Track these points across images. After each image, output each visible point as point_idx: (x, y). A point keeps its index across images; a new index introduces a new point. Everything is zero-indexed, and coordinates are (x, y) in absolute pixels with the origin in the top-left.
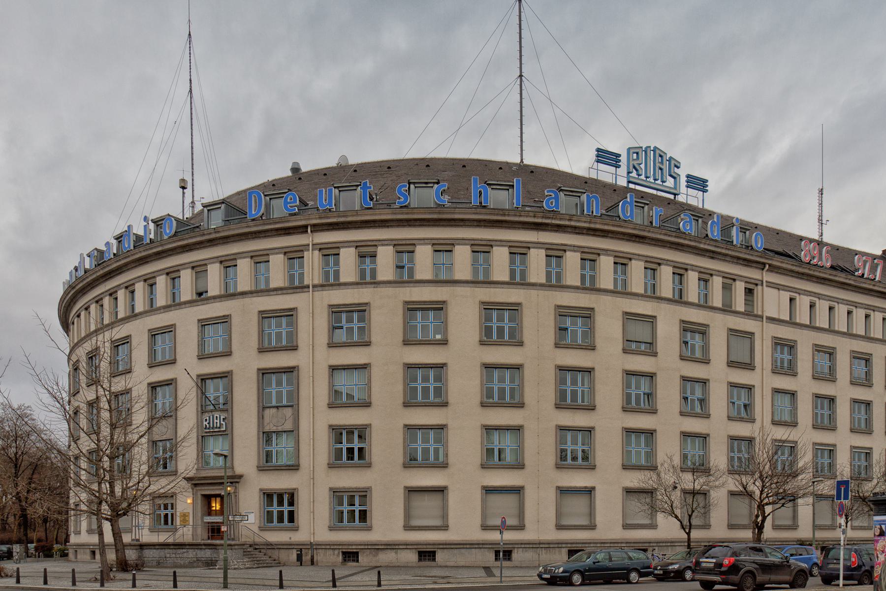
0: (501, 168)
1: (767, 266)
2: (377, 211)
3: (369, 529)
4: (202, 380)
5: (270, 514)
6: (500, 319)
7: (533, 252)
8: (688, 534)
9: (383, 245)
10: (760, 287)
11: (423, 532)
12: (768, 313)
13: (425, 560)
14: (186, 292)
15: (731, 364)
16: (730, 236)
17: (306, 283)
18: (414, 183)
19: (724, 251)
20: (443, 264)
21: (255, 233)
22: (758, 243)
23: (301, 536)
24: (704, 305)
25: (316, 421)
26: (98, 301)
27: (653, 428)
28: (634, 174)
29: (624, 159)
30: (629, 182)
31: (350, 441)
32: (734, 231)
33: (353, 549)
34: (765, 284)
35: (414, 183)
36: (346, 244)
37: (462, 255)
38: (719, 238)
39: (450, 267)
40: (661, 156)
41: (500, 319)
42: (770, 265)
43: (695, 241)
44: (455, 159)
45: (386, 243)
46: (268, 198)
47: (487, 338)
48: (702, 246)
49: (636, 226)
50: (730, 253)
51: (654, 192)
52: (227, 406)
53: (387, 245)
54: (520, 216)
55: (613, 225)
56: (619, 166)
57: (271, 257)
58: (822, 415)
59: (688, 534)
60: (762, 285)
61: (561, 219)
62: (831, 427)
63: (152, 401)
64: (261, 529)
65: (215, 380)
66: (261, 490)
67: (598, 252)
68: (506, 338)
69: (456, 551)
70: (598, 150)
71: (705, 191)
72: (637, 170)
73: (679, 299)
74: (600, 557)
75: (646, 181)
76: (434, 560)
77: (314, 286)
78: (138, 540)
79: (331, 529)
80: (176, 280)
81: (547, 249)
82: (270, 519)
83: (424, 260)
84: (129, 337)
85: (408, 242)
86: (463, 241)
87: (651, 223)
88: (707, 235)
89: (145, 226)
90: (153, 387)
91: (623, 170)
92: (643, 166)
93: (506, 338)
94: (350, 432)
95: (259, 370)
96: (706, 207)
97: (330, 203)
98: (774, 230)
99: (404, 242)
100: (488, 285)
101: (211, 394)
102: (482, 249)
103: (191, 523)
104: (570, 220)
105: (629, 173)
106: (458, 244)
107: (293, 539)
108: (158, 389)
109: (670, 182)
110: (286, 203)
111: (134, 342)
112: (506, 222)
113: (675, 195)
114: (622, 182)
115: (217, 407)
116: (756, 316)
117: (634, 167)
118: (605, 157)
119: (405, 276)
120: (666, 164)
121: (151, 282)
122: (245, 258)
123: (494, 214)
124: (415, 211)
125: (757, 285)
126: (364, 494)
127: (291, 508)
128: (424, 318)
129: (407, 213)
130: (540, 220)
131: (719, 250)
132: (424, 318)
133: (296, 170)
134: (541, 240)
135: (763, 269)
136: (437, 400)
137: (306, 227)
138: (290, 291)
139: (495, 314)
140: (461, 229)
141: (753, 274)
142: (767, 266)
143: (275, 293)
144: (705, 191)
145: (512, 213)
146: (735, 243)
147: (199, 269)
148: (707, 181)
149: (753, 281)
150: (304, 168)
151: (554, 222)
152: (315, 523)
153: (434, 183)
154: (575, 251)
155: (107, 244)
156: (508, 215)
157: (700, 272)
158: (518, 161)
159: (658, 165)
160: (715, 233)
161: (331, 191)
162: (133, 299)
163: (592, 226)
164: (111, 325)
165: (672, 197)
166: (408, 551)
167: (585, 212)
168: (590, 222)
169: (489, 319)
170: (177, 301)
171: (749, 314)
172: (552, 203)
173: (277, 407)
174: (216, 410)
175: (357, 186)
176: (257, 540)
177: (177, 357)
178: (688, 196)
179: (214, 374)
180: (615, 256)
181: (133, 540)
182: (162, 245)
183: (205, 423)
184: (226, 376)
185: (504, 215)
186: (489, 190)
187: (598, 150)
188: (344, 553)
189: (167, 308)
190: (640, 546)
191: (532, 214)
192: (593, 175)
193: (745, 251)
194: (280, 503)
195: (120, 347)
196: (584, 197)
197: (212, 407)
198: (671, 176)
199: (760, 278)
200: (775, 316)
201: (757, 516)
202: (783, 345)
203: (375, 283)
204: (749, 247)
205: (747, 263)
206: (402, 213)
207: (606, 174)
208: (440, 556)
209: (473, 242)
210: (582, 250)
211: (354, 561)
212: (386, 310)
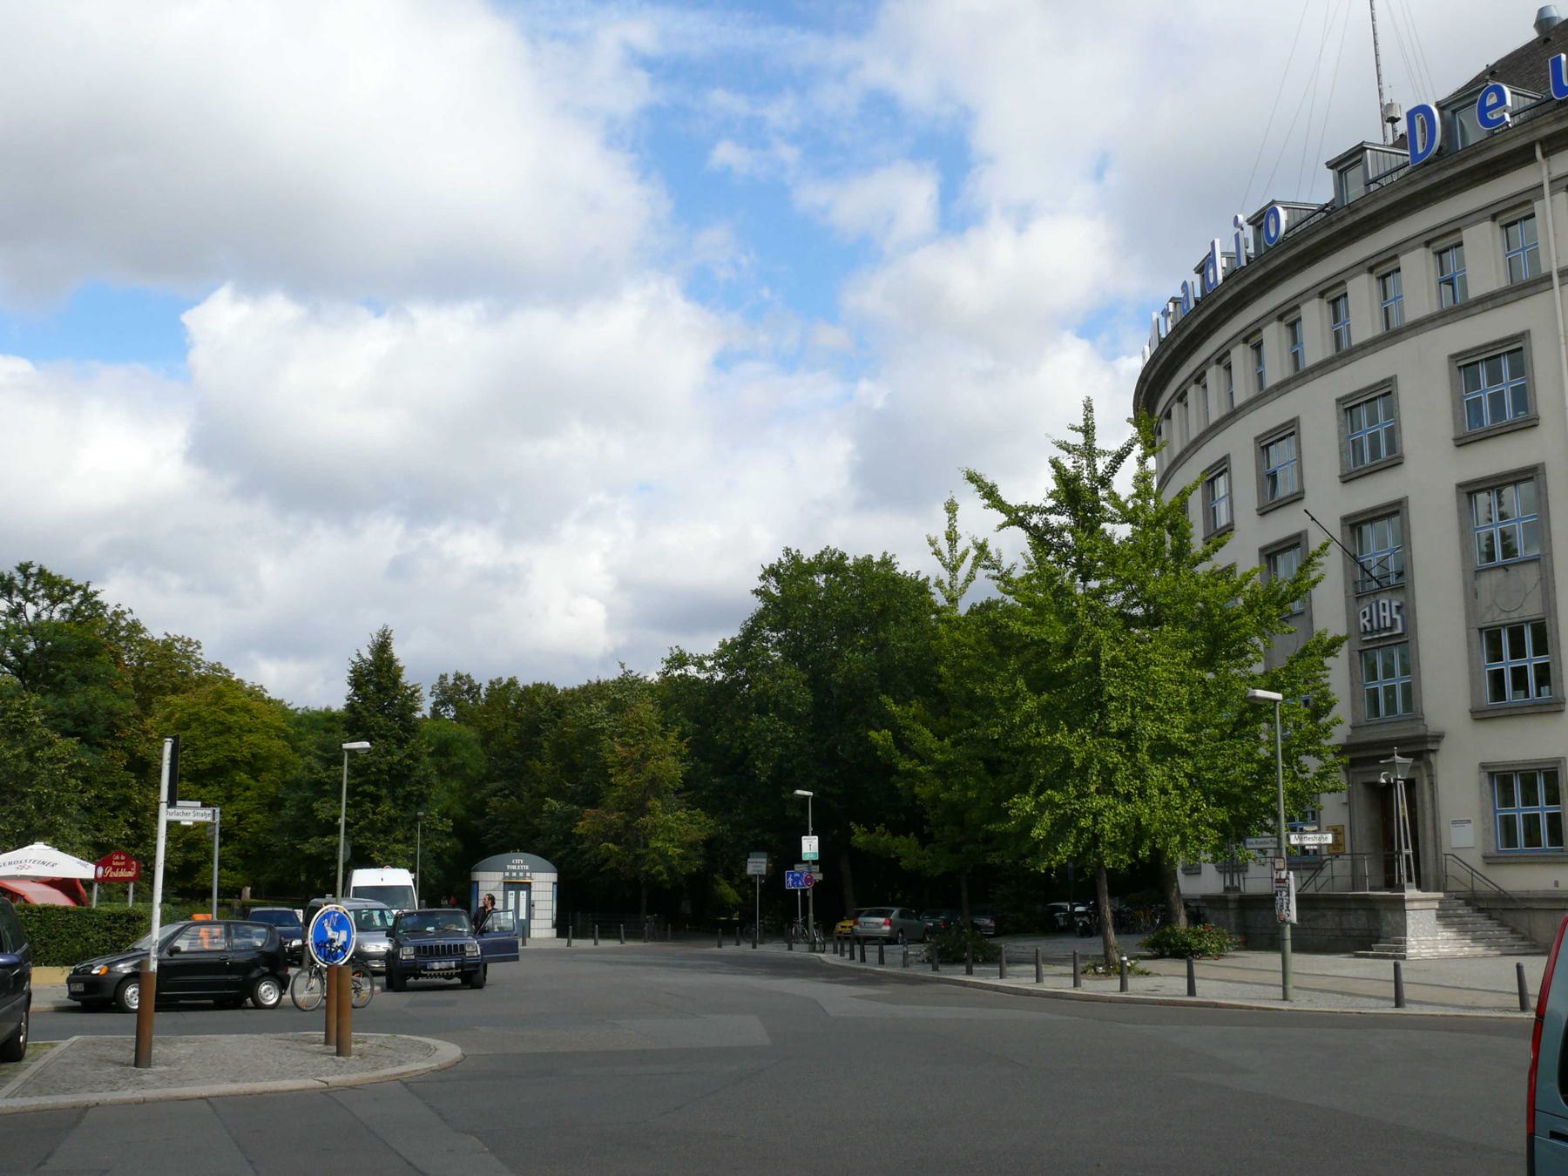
4: (1353, 526)
5: (1508, 824)
14: (1316, 347)
17: (1544, 270)
22: (269, 994)
26: (1222, 358)
52: (1398, 582)
57: (1465, 233)
63: (1353, 559)
64: (1490, 860)
65: (1378, 524)
66: (1483, 766)
74: (703, 818)
78: (1238, 889)
80: (1342, 303)
82: (1510, 839)
84: (1225, 460)
89: (1237, 236)
90: (1355, 524)
94: (1516, 633)
101: (1372, 557)
103: (1348, 850)
107: (1562, 887)
108: (1366, 528)
111: (1236, 465)
121: (1333, 294)
122: (1413, 249)
143: (1480, 308)
147: (1440, 245)
162: (1260, 361)
164: (1324, 367)
170: (1345, 346)
173: (1505, 567)
174: (1382, 589)
176: (1480, 887)
177: (1307, 487)
179: (1373, 510)
181: (1227, 889)
182: (1263, 265)
183: (1364, 621)
195: (1272, 448)
197: (1374, 585)
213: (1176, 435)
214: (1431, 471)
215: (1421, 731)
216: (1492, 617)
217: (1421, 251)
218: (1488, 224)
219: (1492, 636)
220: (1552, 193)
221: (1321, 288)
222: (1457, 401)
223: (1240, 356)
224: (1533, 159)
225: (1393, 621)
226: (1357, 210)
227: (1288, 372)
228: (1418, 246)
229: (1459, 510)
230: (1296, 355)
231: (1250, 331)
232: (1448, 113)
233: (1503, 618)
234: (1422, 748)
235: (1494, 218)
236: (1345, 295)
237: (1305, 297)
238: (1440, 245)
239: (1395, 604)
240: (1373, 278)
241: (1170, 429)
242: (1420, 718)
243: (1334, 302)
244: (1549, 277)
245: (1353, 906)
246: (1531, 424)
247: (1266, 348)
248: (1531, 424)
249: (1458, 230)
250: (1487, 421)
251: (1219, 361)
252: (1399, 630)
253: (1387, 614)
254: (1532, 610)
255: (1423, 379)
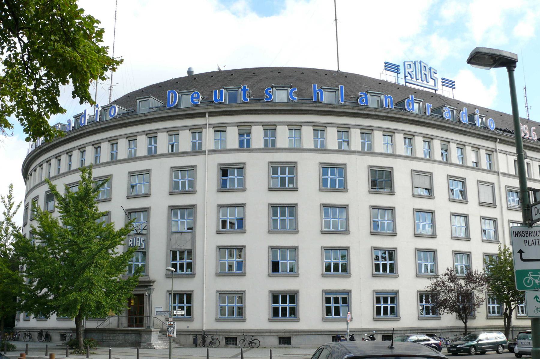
0: (326, 75)
1: (498, 140)
2: (252, 105)
3: (244, 320)
4: (129, 213)
6: (333, 174)
7: (352, 131)
8: (465, 323)
9: (255, 125)
10: (495, 153)
11: (282, 323)
12: (501, 170)
13: (283, 343)
15: (482, 204)
16: (474, 121)
17: (203, 149)
18: (275, 87)
19: (471, 131)
20: (294, 138)
21: (171, 116)
22: (492, 126)
23: (194, 325)
24: (463, 166)
25: (361, 246)
27: (296, 245)
28: (409, 78)
29: (402, 68)
30: (406, 82)
31: (182, 258)
32: (476, 117)
33: (233, 335)
34: (498, 151)
35: (275, 87)
36: (231, 125)
37: (307, 132)
38: (467, 123)
39: (300, 139)
40: (425, 67)
41: (333, 174)
42: (500, 139)
43: (453, 125)
44: (296, 68)
45: (257, 124)
46: (180, 95)
47: (324, 188)
48: (457, 127)
49: (416, 115)
50: (475, 132)
51: (422, 88)
53: (258, 125)
54: (344, 108)
55: (402, 115)
56: (399, 73)
58: (494, 307)
59: (465, 323)
60: (496, 151)
61: (369, 111)
62: (183, 259)
67: (394, 131)
68: (337, 186)
69: (305, 337)
70: (386, 63)
71: (454, 88)
72: (410, 75)
73: (447, 162)
75: (417, 82)
76: (290, 344)
77: (209, 151)
79: (324, 320)
80: (99, 149)
81: (361, 129)
83: (283, 136)
85: (272, 124)
86: (307, 123)
87: (425, 113)
88: (460, 120)
91: (402, 75)
92: (414, 73)
93: (337, 186)
94: (182, 252)
95: (169, 207)
96: (455, 98)
97: (222, 99)
98: (499, 112)
99: (269, 124)
100: (324, 152)
102: (320, 129)
104: (375, 111)
105: (405, 77)
106: (304, 125)
107: (190, 328)
109: (431, 82)
110: (192, 98)
112: (335, 112)
113: (435, 90)
114: (402, 82)
115: (138, 231)
116: (494, 172)
117: (409, 73)
118: (390, 67)
119: (270, 146)
120: (429, 72)
123: (327, 107)
124: (277, 104)
125: (493, 151)
126: (241, 295)
127: (292, 305)
128: (283, 175)
129: (272, 106)
130: (356, 111)
131: (468, 130)
132: (283, 175)
133: (190, 72)
134: (357, 123)
135: (496, 142)
136: (291, 229)
137: (205, 113)
138: (193, 154)
139: (329, 171)
140: (380, 121)
141: (490, 144)
142: (498, 140)
143: (182, 155)
144: (454, 88)
145: (339, 106)
146: (477, 125)
147: (131, 139)
148: (454, 82)
149: (490, 149)
150: (196, 72)
151: (365, 112)
152: (205, 317)
153: (288, 87)
154: (379, 130)
155: (69, 121)
156: (337, 108)
157: (458, 144)
158: (337, 70)
159: (423, 72)
160: (465, 119)
161: (222, 92)
162: (70, 161)
163: (389, 115)
164: (64, 175)
165: (433, 91)
166: (272, 337)
167: (384, 106)
168: (388, 113)
169: (325, 174)
171: (491, 170)
172: (363, 101)
174: (138, 234)
175: (239, 88)
178: (445, 92)
180: (405, 134)
183: (130, 243)
184: (146, 210)
185: (334, 108)
186: (323, 92)
187: (386, 63)
188: (226, 338)
189: (107, 164)
190: (430, 332)
191: (351, 107)
192: (383, 78)
193: (484, 130)
194: (284, 301)
196: (382, 97)
198: (431, 78)
199: (494, 147)
200: (506, 172)
201: (506, 309)
202: (513, 191)
203: (250, 150)
204: (486, 128)
205: (486, 138)
206: (269, 106)
207: (391, 77)
208: (294, 340)
209: (314, 124)
210: (383, 130)
211: (287, 344)
212: (257, 167)
213: (35, 178)
214: (160, 201)
215: (148, 280)
216: (176, 247)
217: (165, 133)
218: (107, 143)
219: (174, 253)
220: (209, 128)
221: (128, 136)
222: (171, 180)
223: (54, 162)
224: (205, 116)
225: (141, 244)
226: (147, 116)
227: (67, 170)
228: (164, 132)
229: (168, 214)
230: (70, 165)
231: (69, 151)
232: (180, 95)
233: (178, 248)
234: (148, 285)
235: (109, 141)
236: (100, 147)
237: (159, 131)
238: (131, 139)
239: (142, 239)
240: (109, 144)
241: (35, 175)
242: (147, 275)
243: (96, 148)
244: (205, 151)
245: (130, 332)
246: (194, 192)
247: (73, 157)
248: (194, 192)
249: (85, 147)
250: (180, 189)
251: (47, 162)
252: (143, 248)
253: (139, 242)
254: (188, 247)
255: (161, 171)
